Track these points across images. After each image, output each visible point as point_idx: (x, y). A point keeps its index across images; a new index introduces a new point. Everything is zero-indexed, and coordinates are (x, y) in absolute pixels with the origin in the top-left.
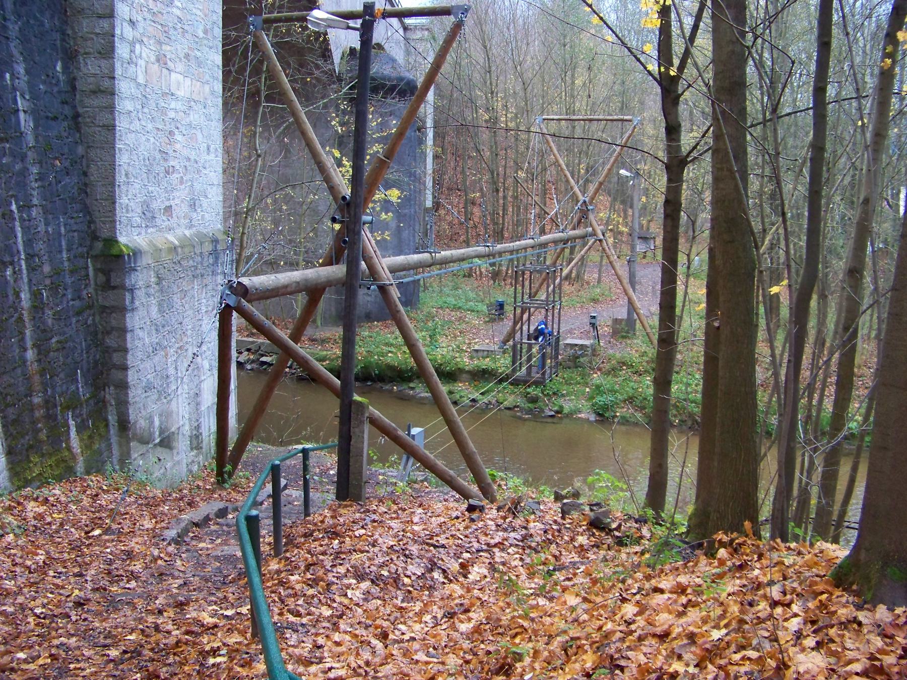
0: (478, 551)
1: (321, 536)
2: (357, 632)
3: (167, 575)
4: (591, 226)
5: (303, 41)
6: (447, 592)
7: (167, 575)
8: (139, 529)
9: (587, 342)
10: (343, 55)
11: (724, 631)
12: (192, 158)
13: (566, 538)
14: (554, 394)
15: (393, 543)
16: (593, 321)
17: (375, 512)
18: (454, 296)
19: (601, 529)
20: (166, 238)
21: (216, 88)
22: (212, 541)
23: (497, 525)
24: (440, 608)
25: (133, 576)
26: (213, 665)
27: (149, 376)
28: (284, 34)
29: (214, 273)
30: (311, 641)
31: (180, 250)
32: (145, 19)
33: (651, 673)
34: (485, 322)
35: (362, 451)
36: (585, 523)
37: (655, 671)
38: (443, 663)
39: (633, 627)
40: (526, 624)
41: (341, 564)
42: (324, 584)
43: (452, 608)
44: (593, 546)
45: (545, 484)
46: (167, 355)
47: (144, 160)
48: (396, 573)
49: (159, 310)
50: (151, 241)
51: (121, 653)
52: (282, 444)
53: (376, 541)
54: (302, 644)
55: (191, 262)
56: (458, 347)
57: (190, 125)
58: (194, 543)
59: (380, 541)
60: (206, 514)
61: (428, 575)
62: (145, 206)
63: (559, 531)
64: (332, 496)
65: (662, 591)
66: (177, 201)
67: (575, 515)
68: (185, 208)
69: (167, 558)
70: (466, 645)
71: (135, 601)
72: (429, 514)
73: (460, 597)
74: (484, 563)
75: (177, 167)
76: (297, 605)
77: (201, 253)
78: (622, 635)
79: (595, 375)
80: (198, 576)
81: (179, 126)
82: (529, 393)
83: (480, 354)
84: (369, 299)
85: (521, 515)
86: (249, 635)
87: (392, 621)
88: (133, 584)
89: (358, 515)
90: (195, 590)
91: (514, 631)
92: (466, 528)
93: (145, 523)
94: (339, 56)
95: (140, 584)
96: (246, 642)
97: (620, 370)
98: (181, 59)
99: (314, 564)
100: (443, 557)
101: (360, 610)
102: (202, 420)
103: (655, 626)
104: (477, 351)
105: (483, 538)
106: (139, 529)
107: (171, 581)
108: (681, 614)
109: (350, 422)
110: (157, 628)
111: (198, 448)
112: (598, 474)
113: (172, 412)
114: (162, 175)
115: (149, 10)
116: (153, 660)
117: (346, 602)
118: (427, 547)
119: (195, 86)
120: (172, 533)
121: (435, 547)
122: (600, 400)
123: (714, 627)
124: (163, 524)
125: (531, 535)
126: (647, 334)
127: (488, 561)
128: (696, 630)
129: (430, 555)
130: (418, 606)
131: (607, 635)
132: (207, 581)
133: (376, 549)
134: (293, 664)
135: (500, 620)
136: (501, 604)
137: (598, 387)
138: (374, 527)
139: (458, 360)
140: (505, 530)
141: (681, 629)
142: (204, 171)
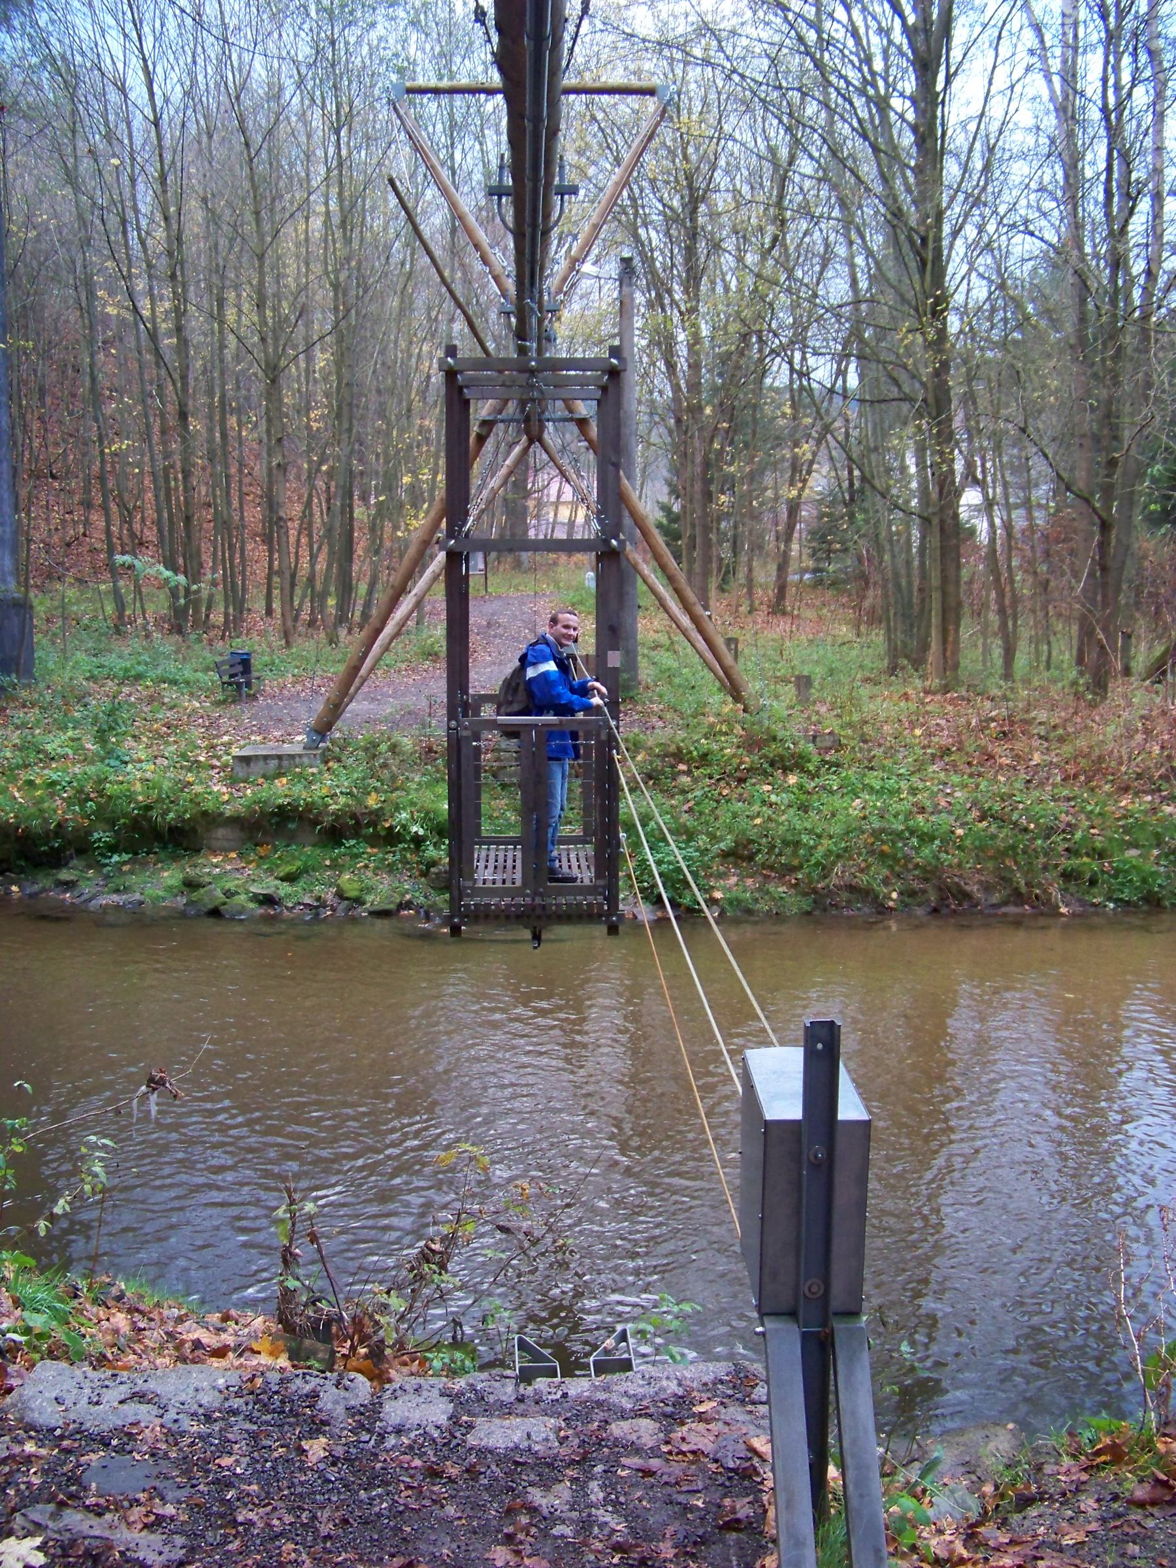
83: (258, 767)
104: (246, 760)
139: (198, 789)
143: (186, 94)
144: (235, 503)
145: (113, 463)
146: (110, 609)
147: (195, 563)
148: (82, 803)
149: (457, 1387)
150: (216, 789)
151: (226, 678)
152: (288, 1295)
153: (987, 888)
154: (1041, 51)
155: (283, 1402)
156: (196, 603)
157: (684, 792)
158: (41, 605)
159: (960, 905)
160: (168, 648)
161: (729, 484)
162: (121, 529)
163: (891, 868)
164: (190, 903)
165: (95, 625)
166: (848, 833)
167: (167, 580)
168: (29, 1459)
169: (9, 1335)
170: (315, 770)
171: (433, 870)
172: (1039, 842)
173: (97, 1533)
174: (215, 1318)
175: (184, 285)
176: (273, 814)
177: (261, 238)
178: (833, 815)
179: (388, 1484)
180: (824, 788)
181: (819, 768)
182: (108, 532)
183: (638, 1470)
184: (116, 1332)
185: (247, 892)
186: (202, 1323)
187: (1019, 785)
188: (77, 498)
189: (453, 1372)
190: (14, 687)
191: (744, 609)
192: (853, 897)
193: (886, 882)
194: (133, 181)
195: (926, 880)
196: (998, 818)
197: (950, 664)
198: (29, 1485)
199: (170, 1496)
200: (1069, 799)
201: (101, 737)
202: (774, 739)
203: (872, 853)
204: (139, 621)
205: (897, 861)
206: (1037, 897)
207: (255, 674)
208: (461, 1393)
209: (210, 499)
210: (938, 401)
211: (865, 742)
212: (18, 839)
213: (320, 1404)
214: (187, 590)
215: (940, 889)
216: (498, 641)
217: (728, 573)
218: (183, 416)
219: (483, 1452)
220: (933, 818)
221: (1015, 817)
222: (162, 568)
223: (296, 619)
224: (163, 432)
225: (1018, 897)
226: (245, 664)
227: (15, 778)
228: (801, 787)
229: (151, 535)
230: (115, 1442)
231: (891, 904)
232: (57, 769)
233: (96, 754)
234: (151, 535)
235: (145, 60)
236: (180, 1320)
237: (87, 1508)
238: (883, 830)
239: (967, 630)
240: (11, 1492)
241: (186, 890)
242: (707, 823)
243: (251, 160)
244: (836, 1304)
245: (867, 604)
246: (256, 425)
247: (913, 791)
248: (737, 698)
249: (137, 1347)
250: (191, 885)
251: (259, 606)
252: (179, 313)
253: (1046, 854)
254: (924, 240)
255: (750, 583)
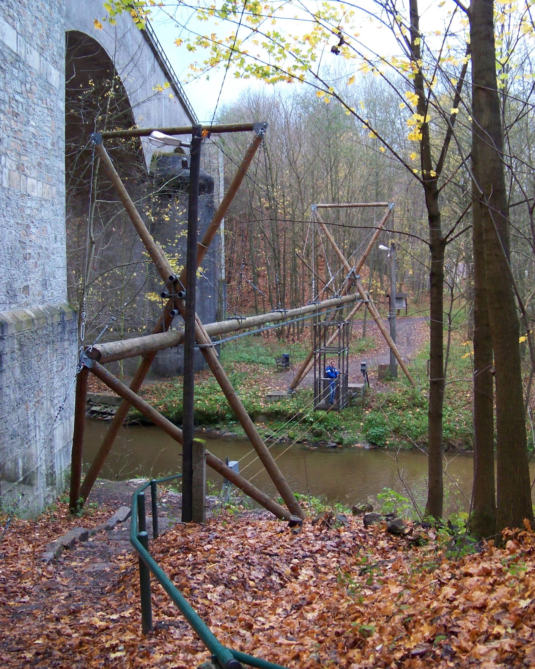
0: (304, 557)
1: (176, 551)
2: (227, 625)
3: (53, 589)
4: (359, 290)
5: (126, 149)
6: (290, 590)
7: (53, 589)
8: (21, 553)
9: (361, 385)
10: (153, 158)
11: (529, 601)
12: (44, 246)
13: (370, 543)
14: (335, 428)
15: (238, 554)
16: (363, 368)
17: (215, 530)
18: (247, 352)
19: (397, 534)
20: (25, 312)
21: (61, 190)
22: (82, 560)
23: (316, 536)
24: (288, 602)
25: (25, 591)
26: (115, 659)
27: (14, 426)
28: (112, 144)
29: (62, 340)
30: (191, 634)
31: (36, 321)
32: (9, 136)
33: (480, 635)
34: (275, 372)
35: (202, 482)
36: (384, 530)
37: (483, 633)
38: (302, 644)
39: (456, 603)
40: (362, 609)
41: (199, 573)
42: (188, 589)
43: (297, 602)
44: (392, 548)
45: (338, 502)
46: (27, 408)
47: (8, 248)
48: (243, 577)
49: (21, 371)
50: (14, 315)
51: (33, 655)
52: (118, 479)
53: (223, 553)
54: (185, 637)
55: (45, 331)
56: (254, 393)
57: (42, 219)
58: (67, 562)
59: (226, 553)
60: (73, 538)
61: (267, 578)
62: (8, 287)
63: (365, 538)
64: (179, 520)
65: (471, 575)
66: (33, 282)
67: (375, 524)
68: (39, 288)
69: (49, 576)
70: (317, 629)
71: (35, 612)
72: (258, 530)
73: (301, 593)
74: (309, 566)
75: (33, 254)
76: (169, 607)
77: (52, 323)
78: (448, 610)
79: (367, 412)
80: (79, 589)
81: (34, 220)
82: (314, 429)
83: (273, 399)
84: (179, 356)
85: (333, 527)
86: (140, 633)
87: (252, 614)
88: (27, 598)
89: (203, 534)
90: (79, 600)
91: (352, 616)
92: (291, 539)
93: (25, 547)
94: (150, 159)
95: (32, 598)
96: (139, 639)
97: (388, 407)
98: (35, 167)
99: (177, 574)
100: (278, 563)
101: (220, 609)
102: (55, 460)
103: (472, 601)
104: (270, 396)
105: (306, 547)
106: (21, 553)
107: (58, 594)
108: (490, 592)
109: (191, 458)
110: (59, 632)
111: (53, 484)
112: (385, 491)
113: (32, 455)
114: (21, 261)
115: (11, 129)
116: (63, 659)
117: (207, 603)
118: (264, 556)
119: (46, 188)
120: (50, 555)
121: (270, 555)
122: (373, 431)
123: (520, 598)
124: (40, 548)
125: (344, 542)
126: (408, 376)
127: (312, 564)
128: (508, 602)
129: (267, 562)
130: (269, 603)
131: (436, 611)
132: (88, 592)
133: (225, 560)
134: (182, 653)
135: (339, 609)
136: (336, 596)
137: (370, 421)
138: (217, 542)
139: (255, 404)
140: (322, 539)
141: (495, 601)
142: (53, 257)
148: (224, 406)
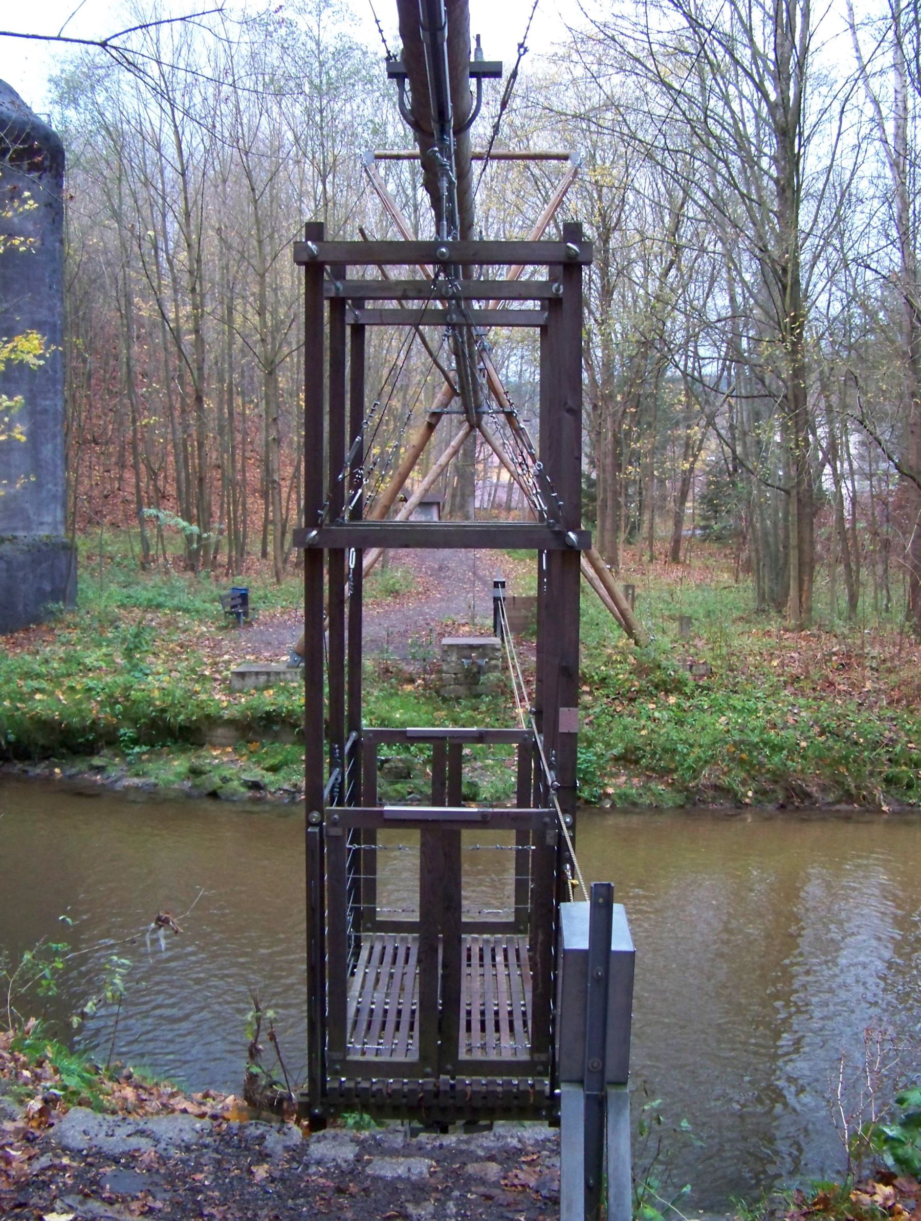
83: (250, 681)
104: (242, 675)
139: (203, 697)
143: (207, 151)
144: (239, 466)
145: (142, 433)
146: (138, 549)
147: (206, 515)
149: (362, 1137)
150: (217, 697)
151: (228, 609)
152: (253, 1078)
153: (824, 789)
154: (878, 122)
155: (240, 1141)
156: (206, 547)
157: (586, 708)
158: (83, 545)
159: (802, 802)
160: (181, 583)
161: (635, 457)
162: (148, 485)
163: (748, 772)
164: (195, 786)
165: (125, 562)
166: (714, 743)
167: (184, 529)
168: (64, 1168)
169: (52, 1090)
170: (295, 684)
171: (386, 765)
172: (866, 753)
173: (110, 1214)
174: (199, 1096)
175: (203, 296)
176: (261, 718)
177: (263, 261)
178: (703, 729)
179: (308, 1196)
180: (697, 707)
181: (693, 692)
182: (138, 486)
183: (484, 1195)
184: (125, 1099)
185: (239, 779)
186: (188, 1098)
187: (852, 707)
188: (113, 459)
189: (359, 1126)
190: (61, 611)
191: (646, 558)
192: (717, 794)
193: (744, 783)
194: (164, 216)
195: (776, 782)
196: (836, 735)
197: (805, 608)
198: (65, 1184)
199: (159, 1196)
200: (892, 719)
201: (128, 654)
202: (659, 667)
203: (732, 759)
204: (161, 560)
205: (752, 766)
206: (864, 797)
207: (251, 606)
208: (365, 1141)
209: (219, 462)
210: (796, 397)
211: (732, 670)
212: (62, 731)
213: (266, 1143)
214: (199, 537)
215: (787, 790)
216: (447, 581)
217: (634, 529)
218: (199, 400)
219: (376, 1179)
220: (782, 733)
221: (847, 733)
222: (180, 520)
223: (285, 561)
224: (183, 411)
225: (849, 797)
226: (244, 598)
227: (60, 685)
228: (678, 706)
229: (171, 490)
230: (123, 1161)
231: (747, 800)
232: (93, 679)
233: (124, 668)
234: (171, 490)
235: (176, 126)
236: (173, 1095)
237: (103, 1199)
238: (742, 742)
239: (821, 581)
240: (53, 1187)
241: (191, 776)
242: (603, 733)
243: (256, 201)
244: (610, 1075)
245: (744, 556)
246: (257, 406)
247: (768, 711)
248: (631, 634)
249: (141, 1112)
250: (195, 772)
251: (258, 548)
252: (197, 318)
253: (872, 763)
254: (785, 270)
255: (651, 539)
